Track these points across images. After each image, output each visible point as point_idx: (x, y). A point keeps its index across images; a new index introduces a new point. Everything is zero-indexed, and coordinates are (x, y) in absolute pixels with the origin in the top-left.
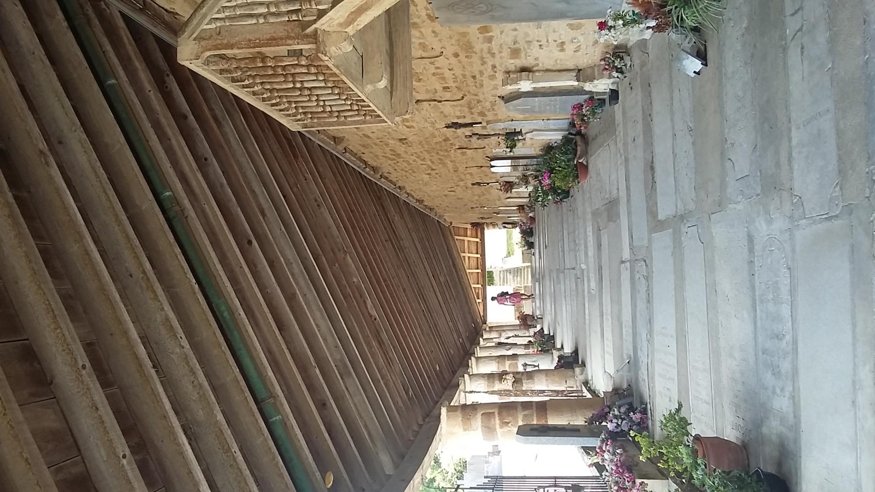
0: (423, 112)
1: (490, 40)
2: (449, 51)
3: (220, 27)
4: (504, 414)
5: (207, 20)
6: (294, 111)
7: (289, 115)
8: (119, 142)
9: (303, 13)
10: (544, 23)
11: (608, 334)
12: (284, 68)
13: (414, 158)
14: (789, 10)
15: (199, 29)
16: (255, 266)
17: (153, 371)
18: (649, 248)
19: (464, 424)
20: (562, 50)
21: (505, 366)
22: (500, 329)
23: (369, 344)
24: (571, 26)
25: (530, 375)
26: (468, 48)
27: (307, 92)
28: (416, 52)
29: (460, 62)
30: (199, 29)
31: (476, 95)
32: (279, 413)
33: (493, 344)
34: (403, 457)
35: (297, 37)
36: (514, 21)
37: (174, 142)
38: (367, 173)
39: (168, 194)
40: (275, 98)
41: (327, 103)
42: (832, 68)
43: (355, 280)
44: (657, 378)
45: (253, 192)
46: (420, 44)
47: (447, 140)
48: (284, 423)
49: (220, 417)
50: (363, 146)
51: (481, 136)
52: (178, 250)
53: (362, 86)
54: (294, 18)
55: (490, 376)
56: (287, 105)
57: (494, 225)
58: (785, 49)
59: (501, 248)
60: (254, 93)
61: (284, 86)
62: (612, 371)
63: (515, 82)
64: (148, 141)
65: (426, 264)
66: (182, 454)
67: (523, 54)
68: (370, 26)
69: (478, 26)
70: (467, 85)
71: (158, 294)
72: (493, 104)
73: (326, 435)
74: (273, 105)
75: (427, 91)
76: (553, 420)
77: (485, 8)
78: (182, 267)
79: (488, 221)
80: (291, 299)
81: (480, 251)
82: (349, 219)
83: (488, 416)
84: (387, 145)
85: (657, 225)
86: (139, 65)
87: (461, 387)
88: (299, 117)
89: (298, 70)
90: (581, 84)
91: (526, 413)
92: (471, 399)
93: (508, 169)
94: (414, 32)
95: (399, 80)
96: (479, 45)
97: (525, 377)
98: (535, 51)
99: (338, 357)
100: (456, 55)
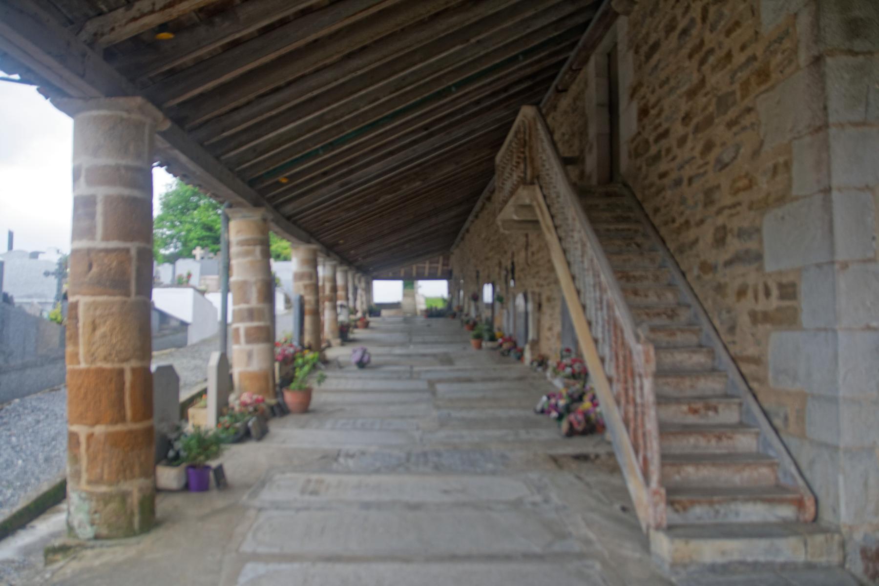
22: (369, 290)
23: (360, 198)
47: (505, 252)
55: (334, 280)
63: (533, 300)
76: (308, 320)
80: (391, 153)
85: (431, 383)
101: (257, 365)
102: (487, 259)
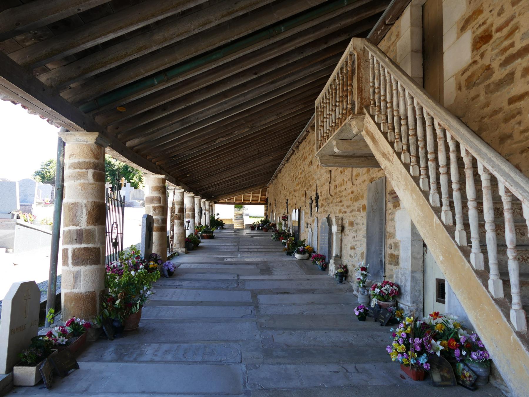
0: (325, 174)
1: (359, 210)
2: (354, 189)
3: (369, 62)
4: (160, 209)
5: (373, 54)
6: (325, 102)
7: (323, 99)
8: (311, 3)
9: (374, 107)
10: (365, 240)
11: (201, 266)
12: (346, 96)
13: (302, 168)
14: (358, 366)
15: (368, 50)
16: (242, 76)
17: (179, 11)
18: (243, 289)
19: (155, 187)
20: (351, 249)
21: (189, 211)
22: (211, 210)
23: (200, 137)
24: (363, 253)
25: (182, 224)
26: (356, 199)
27: (334, 108)
28: (356, 171)
29: (349, 194)
30: (368, 50)
31: (332, 202)
32: (159, 83)
33: (202, 206)
34: (137, 152)
35: (362, 103)
36: (367, 223)
37: (312, 35)
38: (296, 143)
39: (283, 29)
40: (332, 91)
41: (328, 119)
42: (324, 387)
43: (236, 132)
44: (174, 290)
45: (285, 78)
46: (359, 173)
47: (311, 186)
48: (153, 86)
49: (154, 48)
50: (310, 141)
51: (311, 204)
52: (250, 32)
53: (335, 139)
54: (372, 102)
55: (182, 203)
56: (328, 98)
57: (266, 210)
58: (338, 363)
59: (255, 213)
60: (335, 80)
61: (337, 96)
62: (182, 267)
63: (337, 223)
64: (312, 20)
65: (246, 172)
66: (132, 24)
67: (350, 228)
68: (367, 146)
69: (366, 205)
70: (337, 198)
71: (224, 18)
72: (327, 212)
73: (147, 109)
74: (328, 90)
75: (335, 177)
76: (155, 235)
77: (374, 208)
78: (240, 33)
79: (269, 207)
80: (224, 94)
81: (254, 202)
82: (270, 131)
83: (159, 200)
84: (310, 154)
85: (255, 294)
86: (355, 19)
87: (177, 187)
88: (322, 104)
89: (345, 104)
90: (333, 258)
91: (160, 221)
92: (171, 193)
93: (293, 219)
94: (365, 170)
95: (339, 160)
96: (358, 204)
97: (181, 221)
98: (352, 234)
99: (192, 119)
100: (352, 192)
101: (83, 287)
102: (295, 191)
